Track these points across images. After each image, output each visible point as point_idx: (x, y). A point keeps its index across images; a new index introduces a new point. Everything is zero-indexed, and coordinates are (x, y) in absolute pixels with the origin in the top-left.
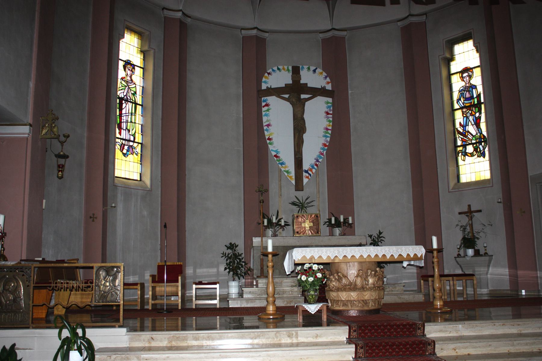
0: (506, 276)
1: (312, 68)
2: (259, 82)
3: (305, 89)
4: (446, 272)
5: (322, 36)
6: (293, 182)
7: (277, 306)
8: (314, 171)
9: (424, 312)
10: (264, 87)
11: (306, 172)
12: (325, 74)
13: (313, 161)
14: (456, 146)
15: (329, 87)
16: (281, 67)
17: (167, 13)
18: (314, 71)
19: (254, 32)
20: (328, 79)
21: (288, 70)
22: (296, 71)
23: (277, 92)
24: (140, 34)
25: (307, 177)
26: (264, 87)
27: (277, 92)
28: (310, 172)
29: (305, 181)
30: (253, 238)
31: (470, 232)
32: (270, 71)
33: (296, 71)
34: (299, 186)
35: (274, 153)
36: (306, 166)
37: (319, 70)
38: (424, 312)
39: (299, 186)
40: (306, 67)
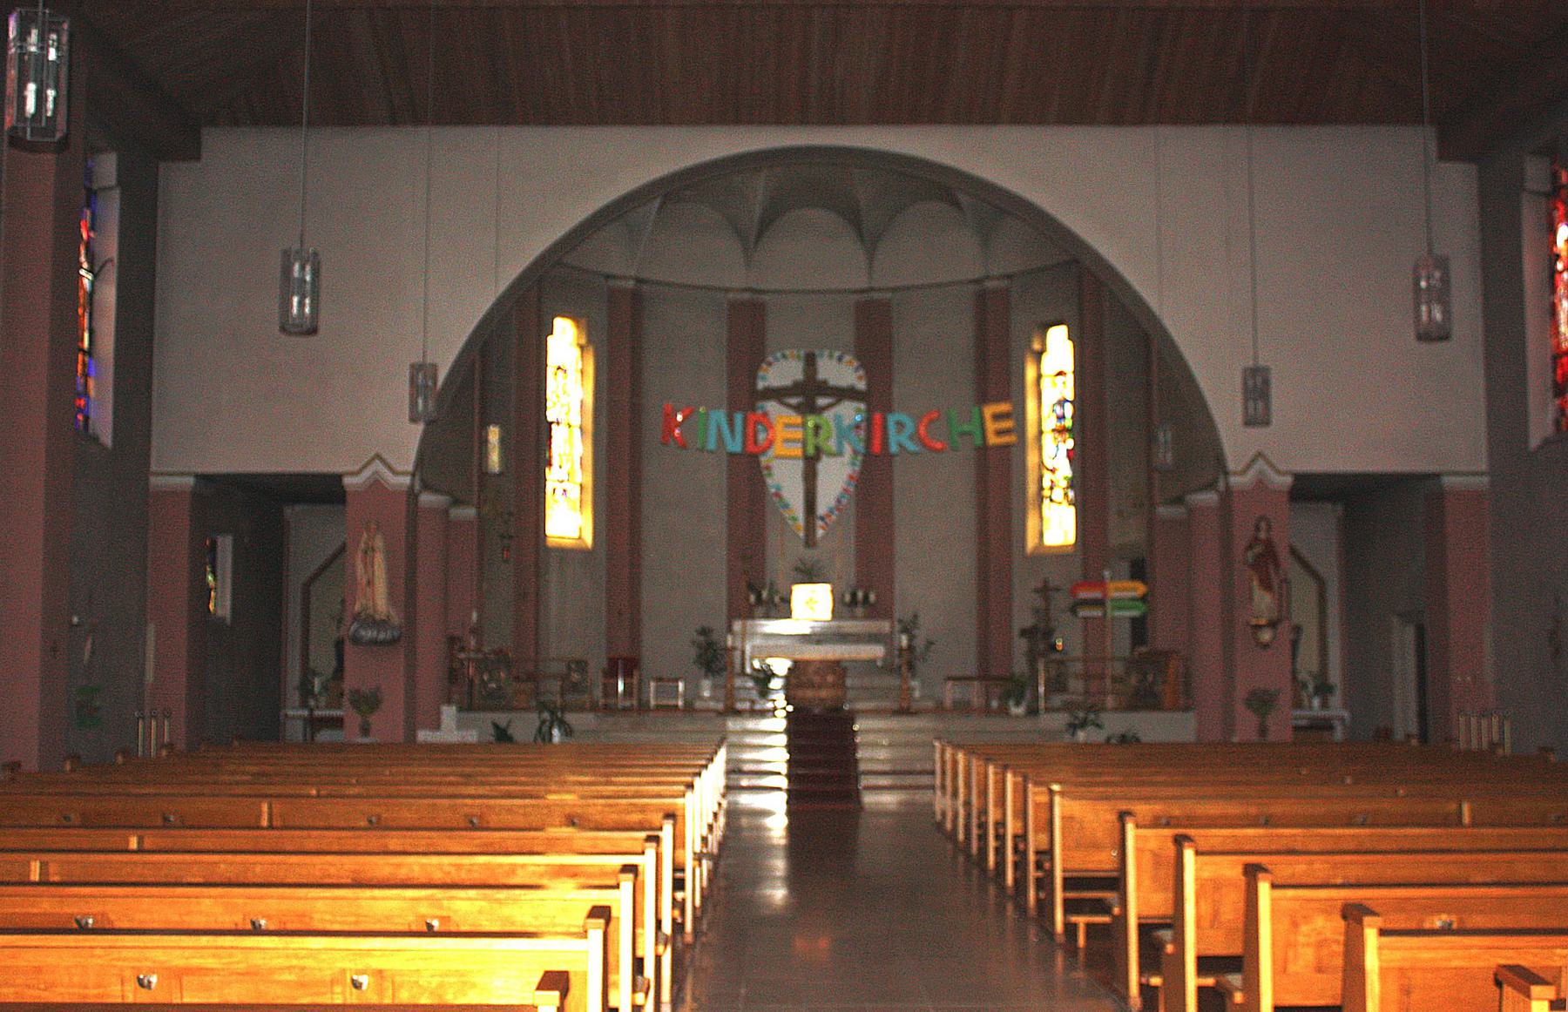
0: (1481, 474)
1: (837, 354)
2: (753, 377)
3: (824, 389)
4: (994, 673)
5: (856, 297)
6: (802, 534)
7: (1064, 729)
8: (834, 517)
9: (1111, 585)
10: (761, 385)
11: (822, 519)
12: (856, 364)
13: (832, 503)
14: (1041, 488)
15: (861, 385)
16: (787, 352)
17: (611, 283)
18: (840, 359)
19: (747, 296)
20: (861, 372)
21: (798, 357)
22: (810, 361)
23: (777, 394)
24: (575, 317)
25: (823, 528)
26: (761, 385)
27: (777, 394)
28: (827, 520)
29: (820, 532)
30: (588, 540)
31: (986, 686)
32: (770, 359)
33: (810, 361)
34: (810, 541)
35: (773, 490)
36: (821, 509)
37: (847, 358)
38: (1111, 585)
39: (810, 541)
40: (826, 353)
